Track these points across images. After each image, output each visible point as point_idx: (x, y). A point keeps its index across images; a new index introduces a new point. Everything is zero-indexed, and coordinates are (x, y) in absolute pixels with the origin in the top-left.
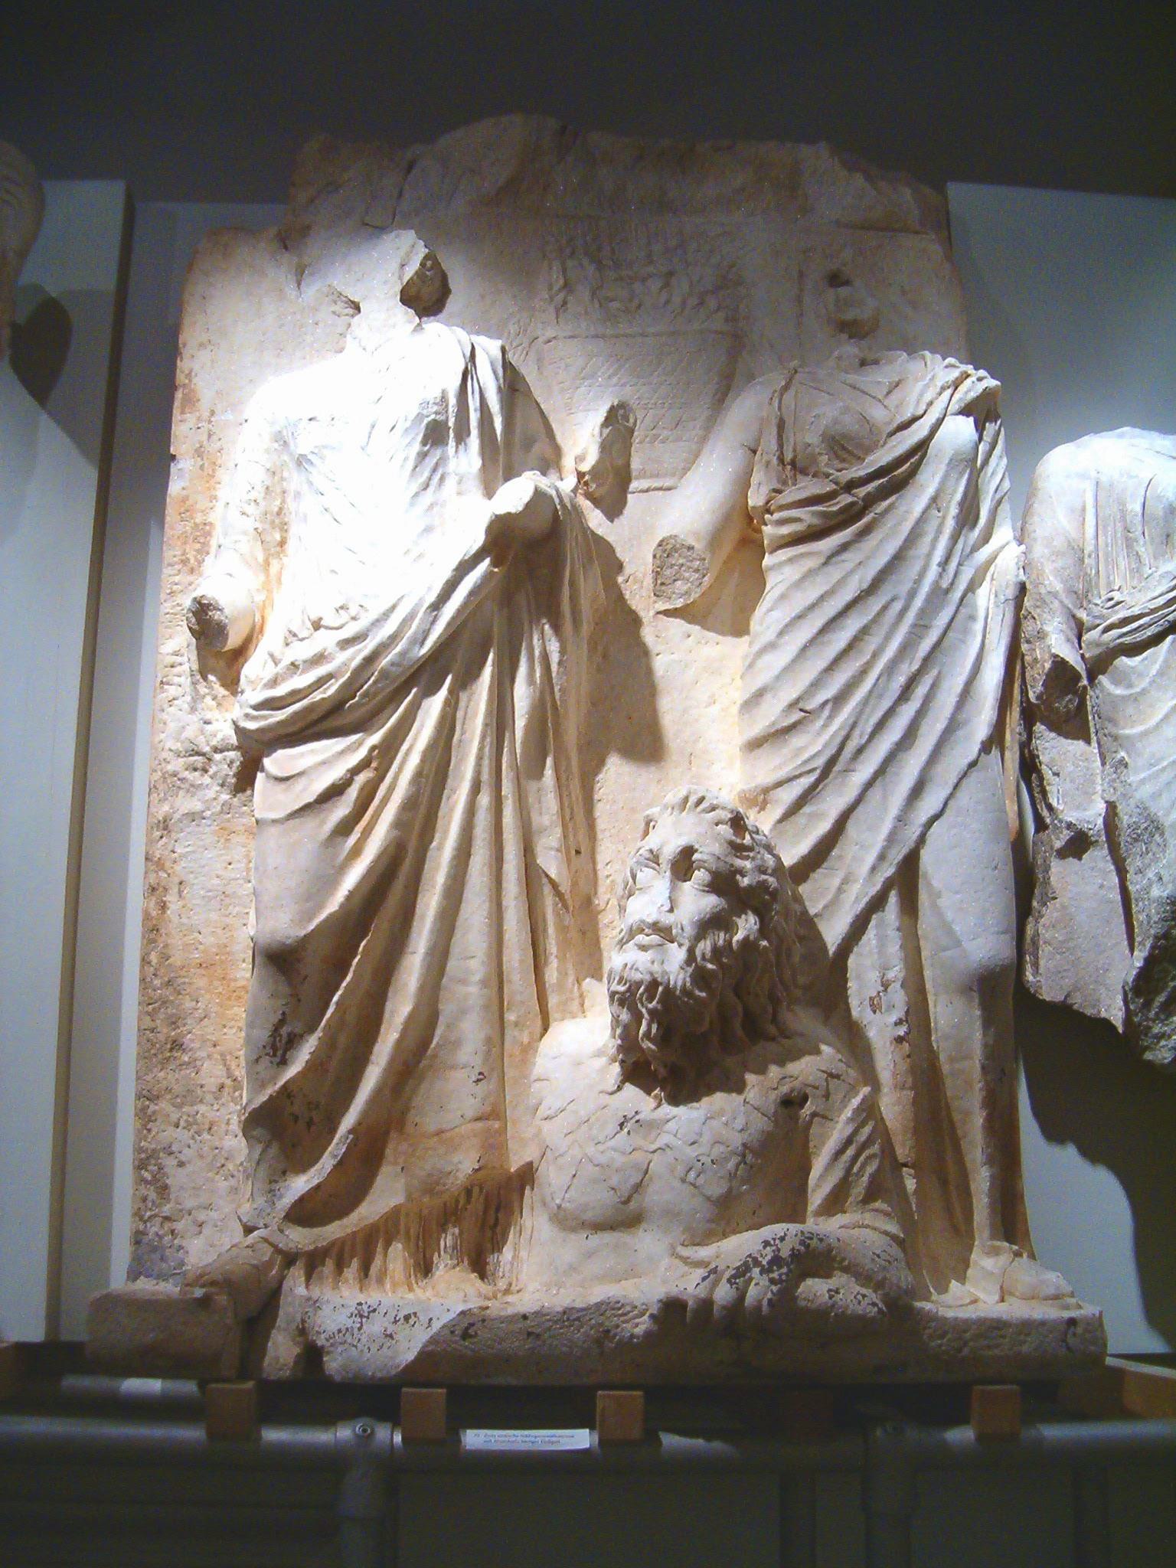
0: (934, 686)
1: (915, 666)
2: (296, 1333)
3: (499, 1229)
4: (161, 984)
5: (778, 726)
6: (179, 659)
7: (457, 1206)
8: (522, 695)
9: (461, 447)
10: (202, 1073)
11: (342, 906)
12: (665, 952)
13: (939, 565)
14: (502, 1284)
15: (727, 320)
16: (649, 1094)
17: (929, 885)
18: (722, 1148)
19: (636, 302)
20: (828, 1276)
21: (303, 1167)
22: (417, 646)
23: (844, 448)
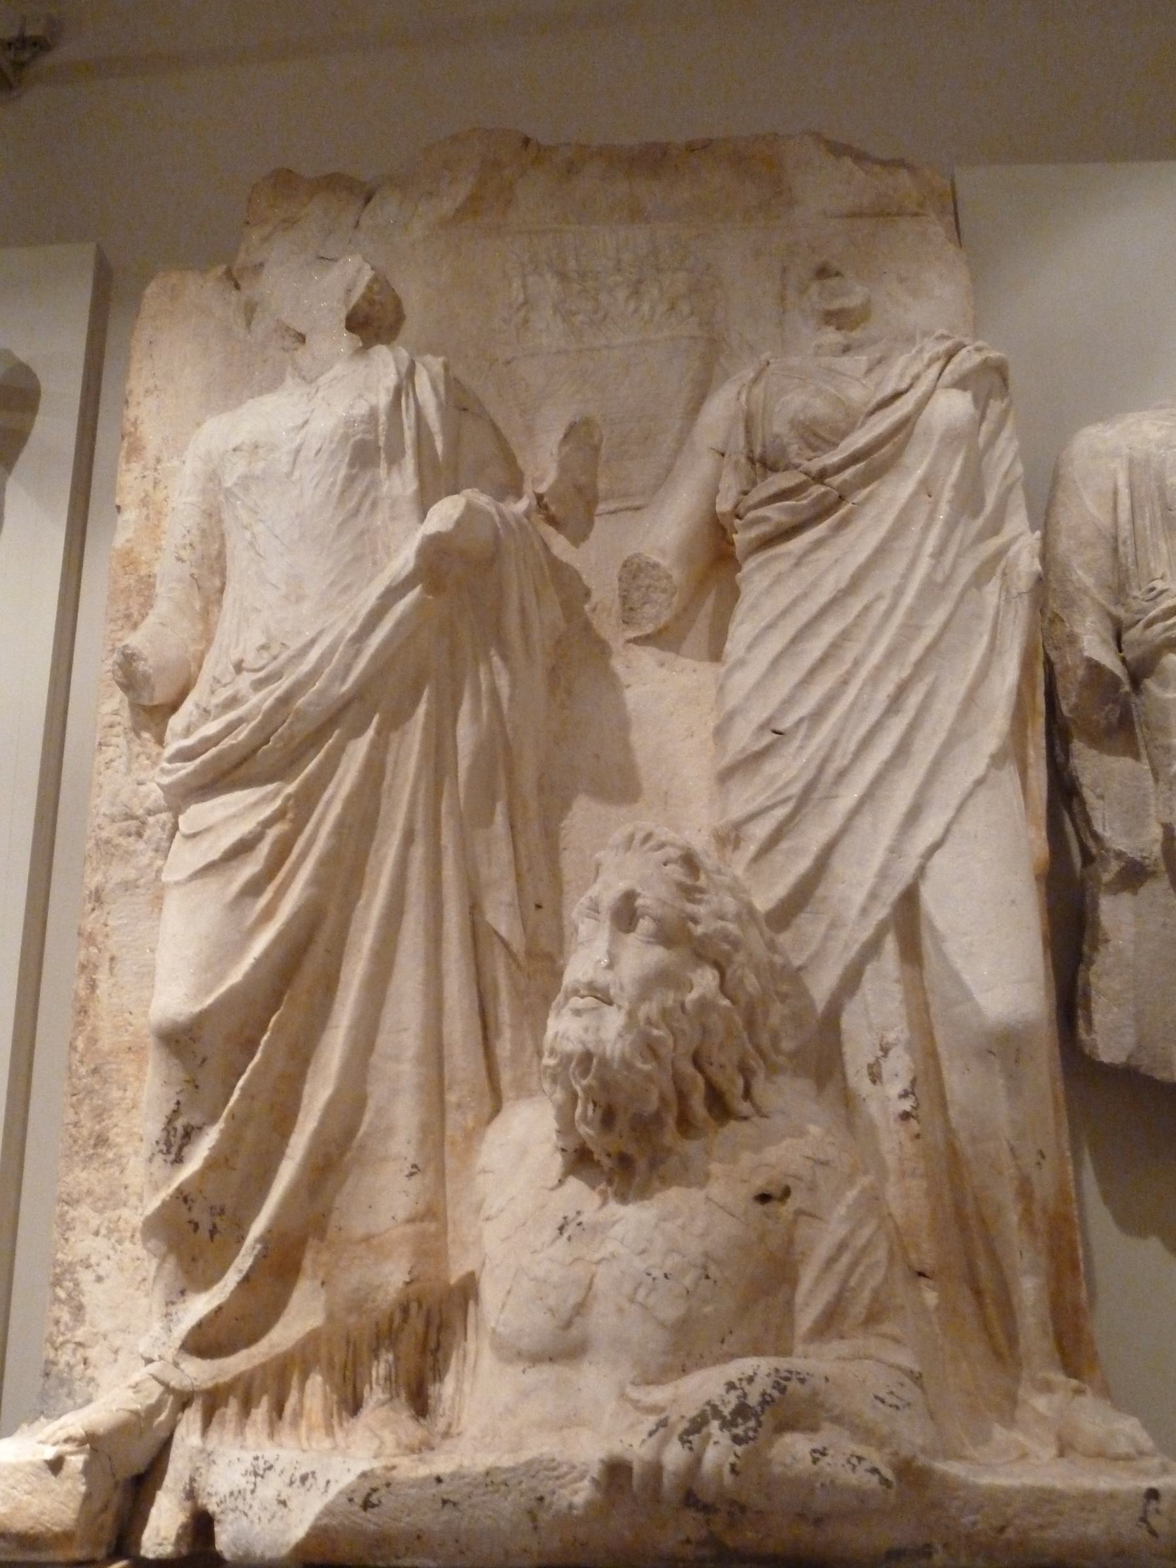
0: (930, 694)
1: (906, 673)
2: (183, 1495)
3: (440, 1355)
4: (87, 1072)
5: (748, 752)
6: (117, 719)
7: (391, 1327)
8: (466, 735)
9: (395, 468)
10: (127, 1172)
11: (247, 976)
12: (601, 1017)
13: (932, 556)
14: (441, 1424)
15: (700, 325)
16: (593, 1188)
17: (933, 929)
18: (677, 1258)
19: (601, 314)
20: (814, 1429)
21: (205, 1283)
22: (337, 684)
23: (816, 435)
